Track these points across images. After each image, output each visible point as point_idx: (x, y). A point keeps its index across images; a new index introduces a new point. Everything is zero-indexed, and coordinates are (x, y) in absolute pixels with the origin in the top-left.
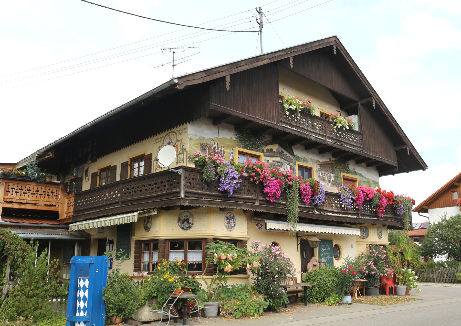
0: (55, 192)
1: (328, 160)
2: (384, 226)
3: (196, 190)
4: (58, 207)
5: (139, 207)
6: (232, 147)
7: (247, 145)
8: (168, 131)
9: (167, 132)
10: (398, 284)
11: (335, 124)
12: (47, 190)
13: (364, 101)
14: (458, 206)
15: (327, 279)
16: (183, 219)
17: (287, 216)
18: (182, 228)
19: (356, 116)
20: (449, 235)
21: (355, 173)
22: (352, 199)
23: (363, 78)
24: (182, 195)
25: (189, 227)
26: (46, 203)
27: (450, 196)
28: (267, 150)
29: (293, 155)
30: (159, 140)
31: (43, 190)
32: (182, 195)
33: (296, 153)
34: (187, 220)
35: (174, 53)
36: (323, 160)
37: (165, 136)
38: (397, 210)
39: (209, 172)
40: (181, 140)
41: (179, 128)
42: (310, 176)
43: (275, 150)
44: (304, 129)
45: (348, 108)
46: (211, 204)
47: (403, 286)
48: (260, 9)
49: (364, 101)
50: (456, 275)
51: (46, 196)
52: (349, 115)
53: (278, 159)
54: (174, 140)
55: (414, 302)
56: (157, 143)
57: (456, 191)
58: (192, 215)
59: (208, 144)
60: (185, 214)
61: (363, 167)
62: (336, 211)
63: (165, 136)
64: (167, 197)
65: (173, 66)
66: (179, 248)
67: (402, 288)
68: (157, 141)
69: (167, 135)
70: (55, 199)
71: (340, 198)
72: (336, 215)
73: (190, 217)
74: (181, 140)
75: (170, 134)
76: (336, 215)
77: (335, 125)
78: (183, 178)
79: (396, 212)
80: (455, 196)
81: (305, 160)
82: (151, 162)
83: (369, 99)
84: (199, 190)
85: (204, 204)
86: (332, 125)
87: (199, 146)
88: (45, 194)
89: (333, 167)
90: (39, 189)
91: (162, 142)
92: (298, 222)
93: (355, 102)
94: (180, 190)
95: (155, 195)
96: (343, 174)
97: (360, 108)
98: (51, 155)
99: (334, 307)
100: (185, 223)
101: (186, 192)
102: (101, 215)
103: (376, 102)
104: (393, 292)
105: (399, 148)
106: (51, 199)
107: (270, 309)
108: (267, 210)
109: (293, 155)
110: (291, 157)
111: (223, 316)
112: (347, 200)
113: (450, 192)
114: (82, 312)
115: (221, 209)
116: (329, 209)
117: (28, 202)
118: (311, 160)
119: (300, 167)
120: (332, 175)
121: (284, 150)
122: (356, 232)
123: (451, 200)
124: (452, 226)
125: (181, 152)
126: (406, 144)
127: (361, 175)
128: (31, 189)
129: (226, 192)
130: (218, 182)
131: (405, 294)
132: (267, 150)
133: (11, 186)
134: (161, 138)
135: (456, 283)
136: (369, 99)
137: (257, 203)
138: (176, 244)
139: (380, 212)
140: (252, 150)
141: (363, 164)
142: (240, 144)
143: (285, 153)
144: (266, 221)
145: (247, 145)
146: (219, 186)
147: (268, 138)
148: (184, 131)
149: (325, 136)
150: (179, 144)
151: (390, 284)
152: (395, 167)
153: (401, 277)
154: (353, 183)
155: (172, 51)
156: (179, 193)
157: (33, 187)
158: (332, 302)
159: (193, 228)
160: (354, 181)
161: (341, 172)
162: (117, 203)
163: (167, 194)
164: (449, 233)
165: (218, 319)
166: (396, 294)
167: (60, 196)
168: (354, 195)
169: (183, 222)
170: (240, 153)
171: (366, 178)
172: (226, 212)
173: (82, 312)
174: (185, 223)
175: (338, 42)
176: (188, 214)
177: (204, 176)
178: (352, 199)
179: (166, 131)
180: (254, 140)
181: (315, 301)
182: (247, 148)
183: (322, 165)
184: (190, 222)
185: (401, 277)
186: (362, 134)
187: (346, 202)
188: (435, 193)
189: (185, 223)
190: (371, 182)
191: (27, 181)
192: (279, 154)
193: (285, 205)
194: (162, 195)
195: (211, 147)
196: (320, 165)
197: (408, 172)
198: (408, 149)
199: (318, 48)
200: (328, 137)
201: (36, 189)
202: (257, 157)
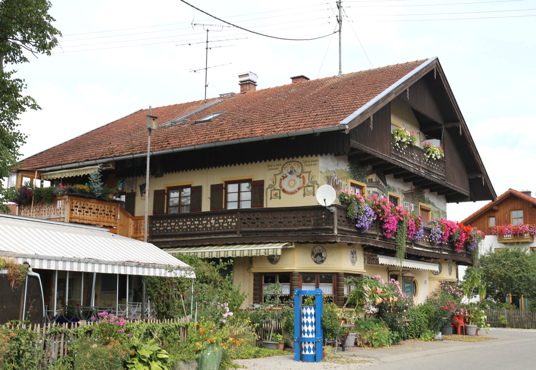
0: (113, 211)
1: (409, 189)
2: (453, 261)
3: (342, 226)
4: (116, 229)
5: (272, 239)
6: (346, 179)
7: (356, 176)
8: (288, 159)
9: (286, 160)
10: (468, 323)
11: (428, 154)
12: (106, 209)
13: (449, 125)
14: (495, 234)
15: (420, 316)
16: (316, 253)
17: (395, 251)
18: (316, 262)
19: (439, 141)
20: (496, 271)
21: (429, 202)
22: (441, 234)
23: (455, 102)
24: (336, 232)
25: (322, 261)
26: (106, 224)
27: (486, 221)
28: (369, 180)
29: (386, 184)
30: (275, 167)
31: (103, 208)
32: (336, 232)
33: (388, 182)
34: (320, 254)
35: (208, 31)
36: (407, 189)
37: (284, 164)
38: (470, 244)
39: (354, 210)
40: (309, 172)
41: (310, 158)
42: (396, 204)
43: (374, 180)
44: (406, 160)
45: (429, 130)
46: (352, 240)
47: (473, 325)
48: (340, 3)
49: (449, 125)
50: (499, 318)
51: (105, 216)
52: (428, 138)
53: (376, 190)
54: (299, 171)
55: (492, 340)
56: (270, 169)
57: (494, 217)
58: (324, 250)
59: (331, 177)
60: (318, 248)
61: (435, 195)
62: (427, 246)
63: (284, 164)
64: (312, 232)
65: (207, 48)
66: (310, 282)
67: (472, 328)
68: (270, 168)
69: (287, 163)
70: (113, 220)
71: (430, 233)
72: (425, 250)
73: (323, 251)
74: (309, 172)
75: (293, 163)
76: (425, 250)
77: (428, 154)
78: (336, 217)
79: (469, 247)
80: (492, 222)
81: (394, 190)
82: (263, 189)
83: (456, 125)
84: (345, 227)
85: (348, 240)
86: (425, 154)
87: (326, 179)
88: (104, 213)
89: (413, 196)
90: (99, 208)
91: (280, 170)
92: (405, 258)
93: (439, 125)
94: (334, 227)
95: (296, 229)
96: (421, 204)
97: (444, 131)
98: (111, 167)
99: (429, 342)
100: (319, 257)
101: (338, 230)
102: (205, 244)
103: (462, 129)
104: (465, 331)
105: (473, 177)
106: (109, 219)
107: (395, 342)
108: (384, 246)
109: (386, 184)
110: (385, 187)
111: (360, 346)
112: (437, 235)
113: (486, 216)
114: (310, 334)
115: (349, 244)
116: (422, 244)
117: (90, 222)
118: (397, 189)
119: (391, 197)
120: (412, 205)
121: (380, 180)
122: (436, 268)
123: (486, 227)
124: (497, 261)
125: (309, 184)
126: (481, 173)
127: (433, 204)
128: (92, 207)
129: (362, 228)
130: (356, 220)
131: (474, 334)
132: (369, 180)
133: (74, 205)
134: (277, 165)
135: (499, 327)
136: (456, 125)
137: (377, 239)
138: (308, 277)
139: (459, 247)
140: (359, 181)
141: (436, 193)
142: (351, 175)
143: (381, 182)
144: (378, 256)
145: (356, 176)
146: (357, 223)
147: (369, 168)
148: (315, 163)
149: (420, 167)
150: (306, 175)
151: (461, 323)
152: (467, 197)
153: (473, 317)
154: (426, 213)
155: (206, 28)
156: (332, 230)
157: (93, 205)
158: (429, 338)
159: (325, 262)
160: (428, 211)
161: (419, 201)
162: (234, 233)
163: (313, 230)
164: (496, 270)
165: (356, 348)
166: (466, 334)
167: (119, 215)
168: (442, 230)
169: (316, 256)
170: (352, 185)
171: (437, 208)
172: (351, 247)
173: (310, 334)
174: (318, 257)
175: (438, 64)
176: (321, 248)
177: (349, 214)
178: (441, 234)
179: (286, 159)
180: (360, 170)
181: (410, 337)
182: (355, 180)
183: (406, 194)
184: (323, 255)
185: (473, 317)
186: (445, 162)
187: (436, 237)
188: (469, 217)
189: (319, 257)
190: (441, 212)
191: (90, 198)
192: (377, 185)
193: (394, 240)
194: (308, 230)
195: (333, 180)
196: (404, 194)
197: (474, 202)
198: (483, 178)
199: (425, 73)
200: (422, 168)
201: (96, 207)
202: (361, 188)
